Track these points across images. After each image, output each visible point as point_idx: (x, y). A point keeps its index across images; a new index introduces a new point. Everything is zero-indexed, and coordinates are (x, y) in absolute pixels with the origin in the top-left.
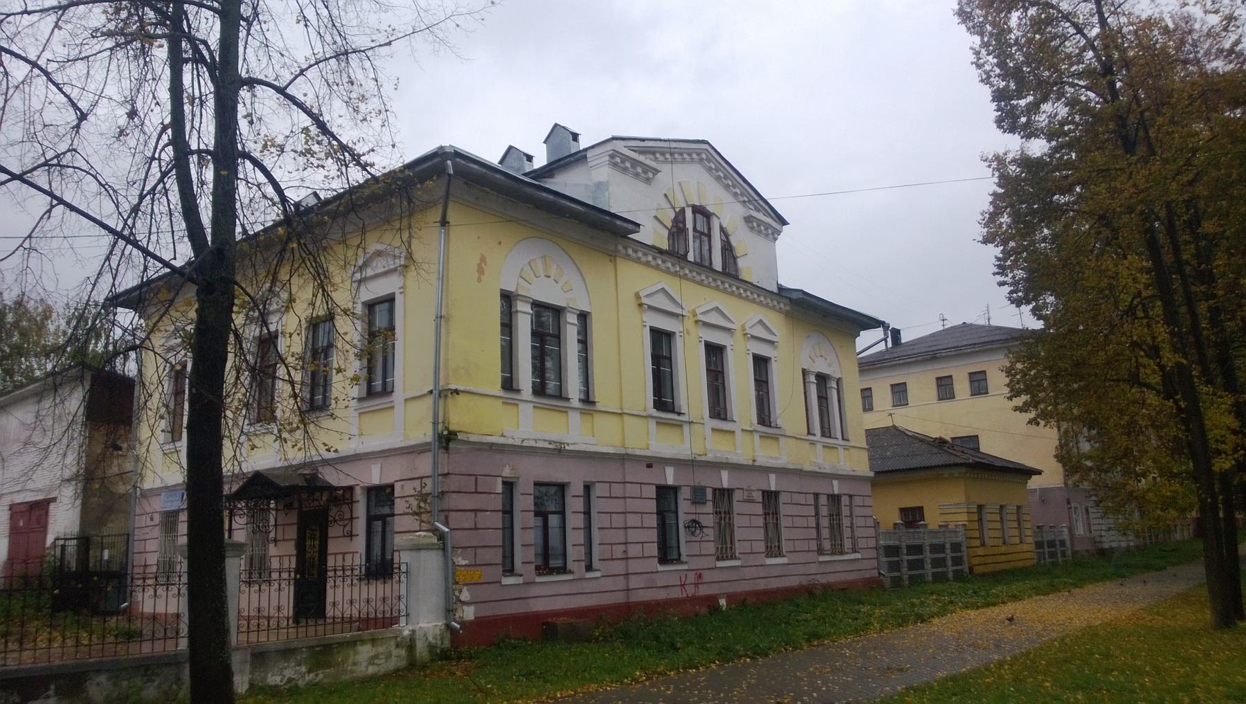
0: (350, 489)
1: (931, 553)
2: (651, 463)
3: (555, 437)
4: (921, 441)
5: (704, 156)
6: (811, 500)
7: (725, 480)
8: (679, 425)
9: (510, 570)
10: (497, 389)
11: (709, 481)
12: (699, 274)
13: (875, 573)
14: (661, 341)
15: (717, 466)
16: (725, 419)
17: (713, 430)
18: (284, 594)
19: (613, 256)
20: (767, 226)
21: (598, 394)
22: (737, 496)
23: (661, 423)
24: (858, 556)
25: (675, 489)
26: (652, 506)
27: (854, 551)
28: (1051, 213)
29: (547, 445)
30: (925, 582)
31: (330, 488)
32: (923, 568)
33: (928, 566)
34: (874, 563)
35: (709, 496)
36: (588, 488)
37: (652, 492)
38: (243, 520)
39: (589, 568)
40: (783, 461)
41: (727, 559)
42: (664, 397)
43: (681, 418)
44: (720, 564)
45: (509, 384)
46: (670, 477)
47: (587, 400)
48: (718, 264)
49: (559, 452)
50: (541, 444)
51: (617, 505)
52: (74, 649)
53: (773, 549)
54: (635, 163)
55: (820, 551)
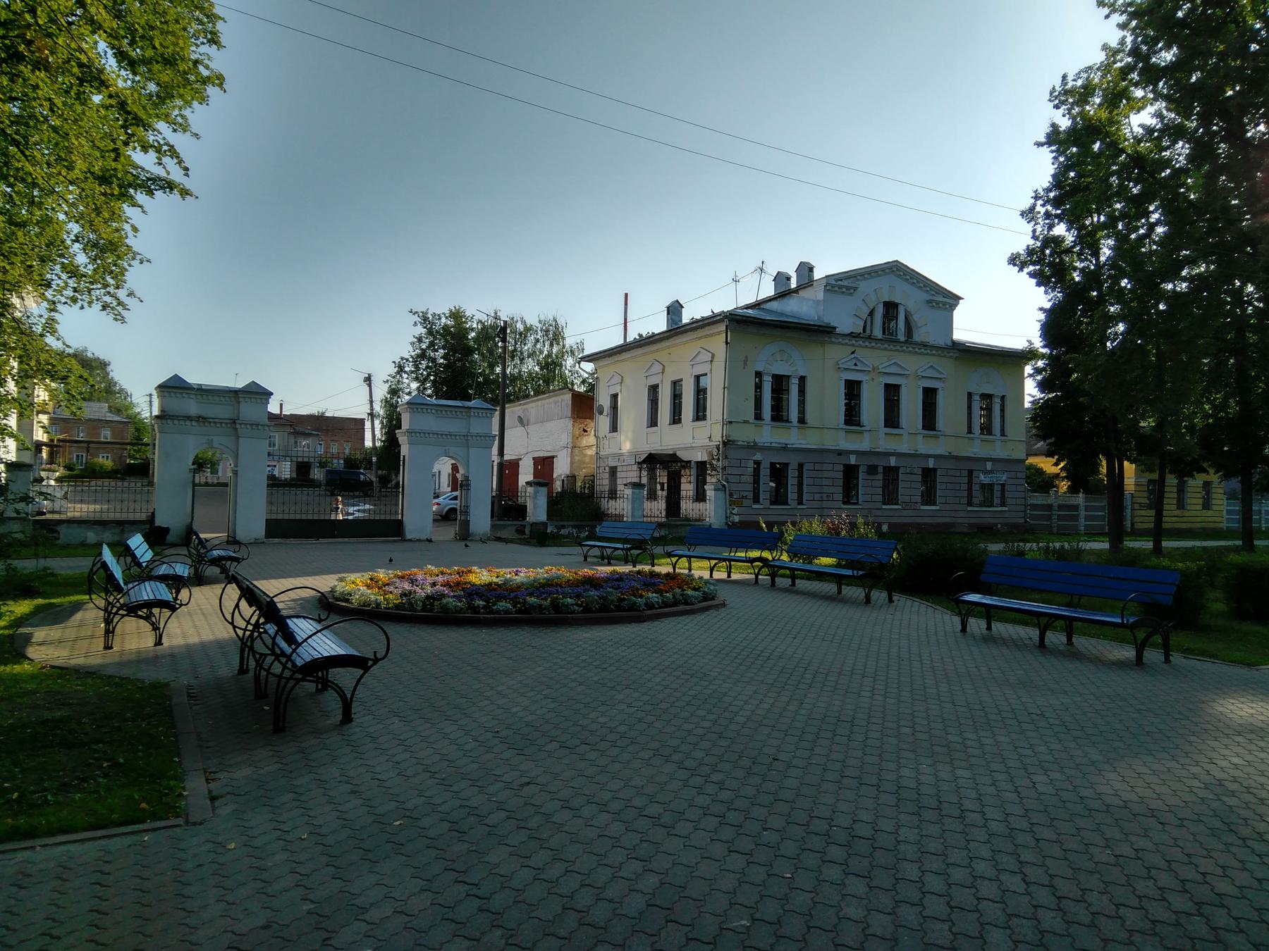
0: (690, 462)
1: (1086, 511)
2: (840, 453)
3: (783, 441)
4: (231, 391)
5: (895, 269)
6: (966, 473)
7: (893, 462)
8: (937, 437)
9: (756, 499)
10: (752, 419)
11: (881, 463)
12: (895, 346)
13: (1022, 520)
14: (853, 390)
15: (887, 454)
16: (898, 427)
17: (886, 434)
18: (684, 508)
19: (822, 344)
20: (944, 303)
21: (1008, 430)
22: (901, 470)
23: (847, 432)
24: (1006, 509)
25: (856, 467)
26: (841, 475)
27: (1003, 504)
28: (1049, 278)
29: (777, 445)
30: (1079, 534)
31: (681, 461)
32: (1077, 520)
33: (1082, 521)
34: (1022, 514)
35: (880, 470)
36: (801, 466)
37: (841, 468)
38: (646, 473)
39: (800, 503)
40: (940, 451)
41: (888, 504)
42: (852, 416)
43: (863, 428)
44: (884, 507)
45: (758, 416)
46: (853, 460)
47: (802, 420)
48: (902, 338)
49: (784, 448)
50: (773, 445)
51: (816, 474)
52: (789, 682)
53: (758, 463)
54: (840, 287)
55: (970, 503)
